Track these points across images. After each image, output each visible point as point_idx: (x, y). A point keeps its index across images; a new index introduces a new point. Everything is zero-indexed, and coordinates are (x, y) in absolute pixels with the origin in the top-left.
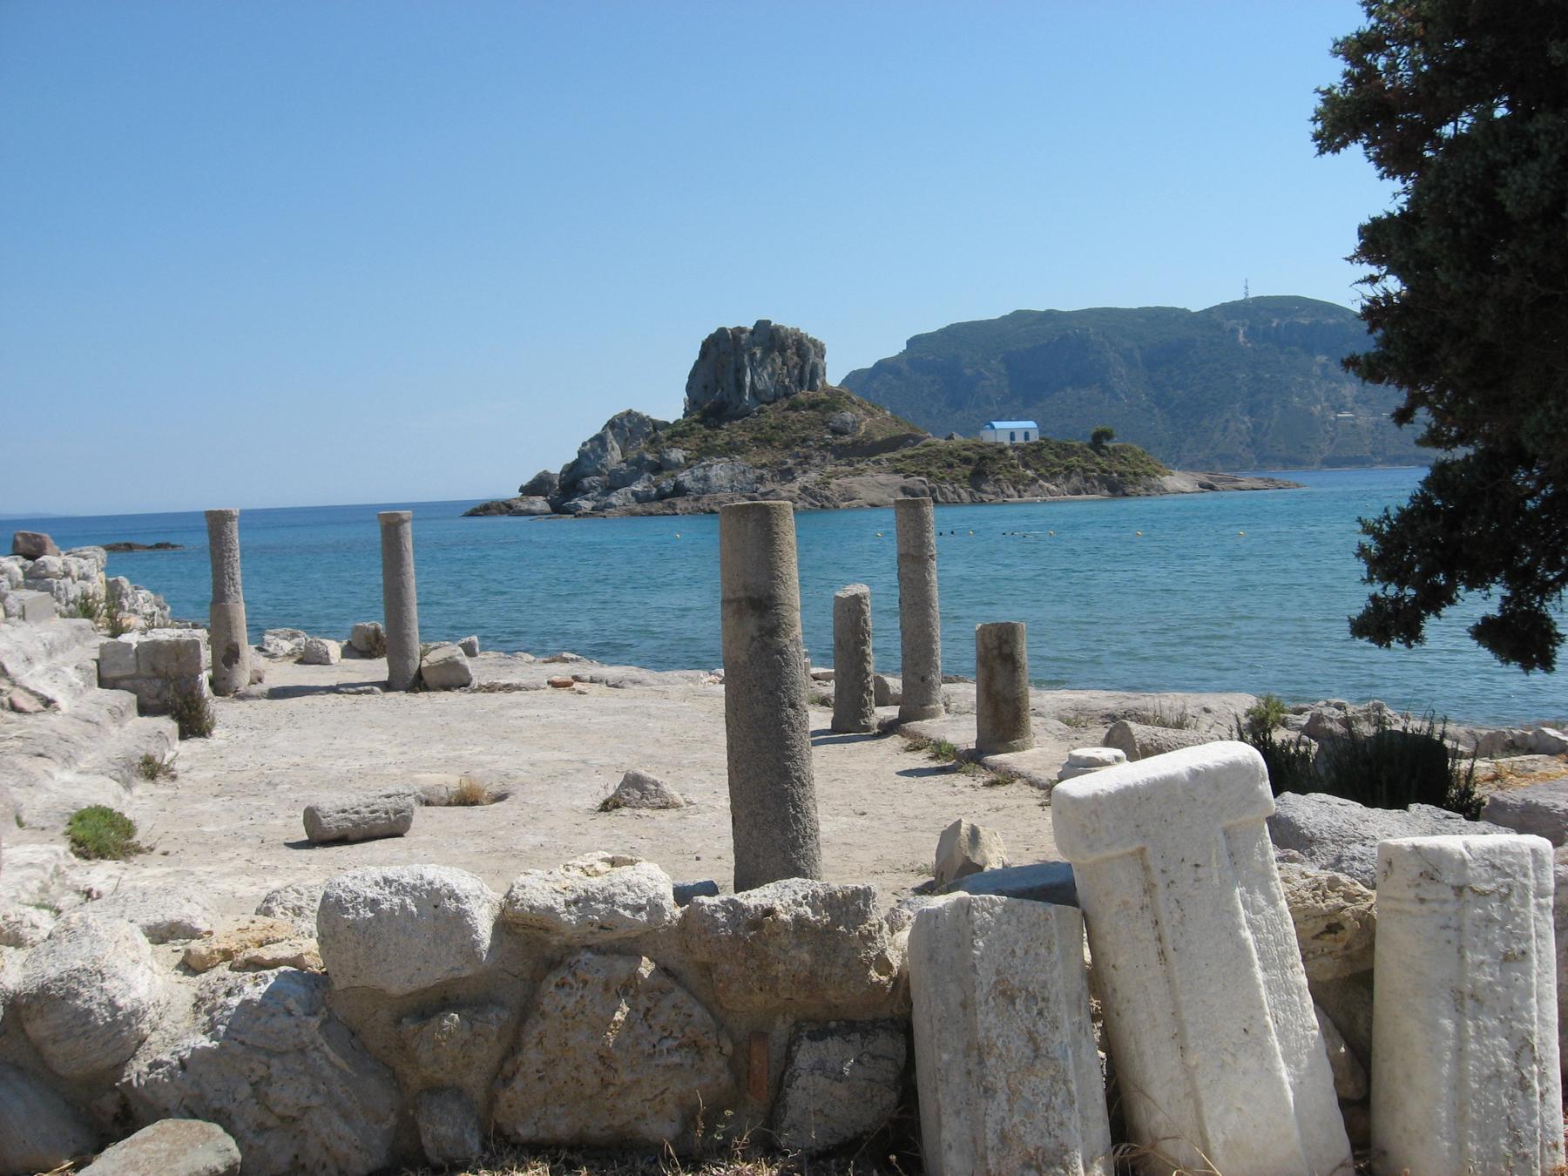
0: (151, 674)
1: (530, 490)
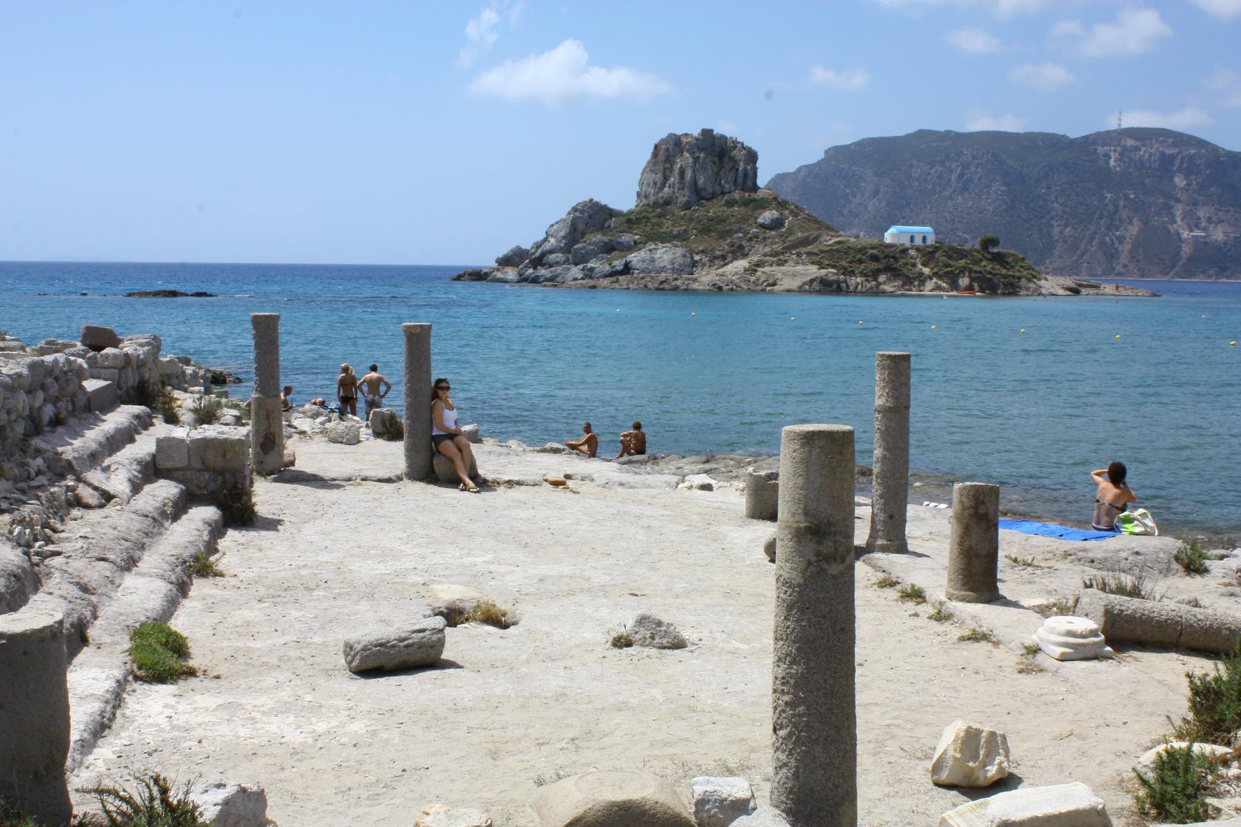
0: (200, 466)
1: (505, 262)
